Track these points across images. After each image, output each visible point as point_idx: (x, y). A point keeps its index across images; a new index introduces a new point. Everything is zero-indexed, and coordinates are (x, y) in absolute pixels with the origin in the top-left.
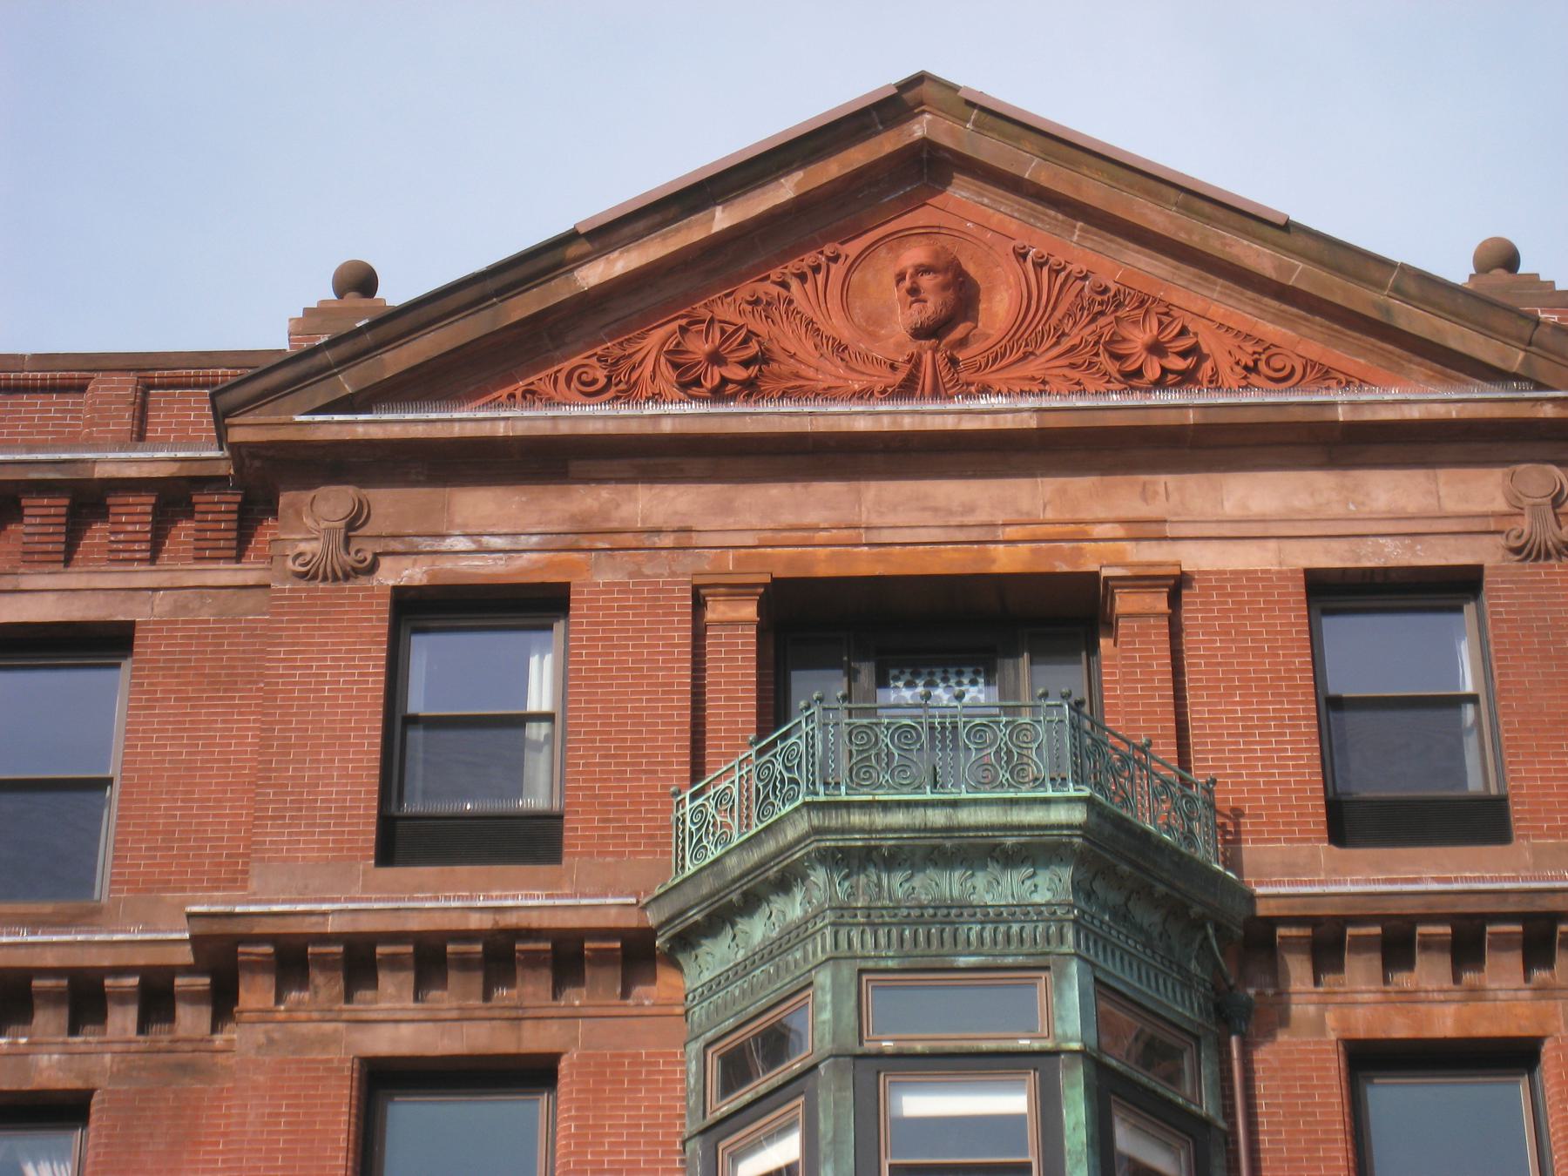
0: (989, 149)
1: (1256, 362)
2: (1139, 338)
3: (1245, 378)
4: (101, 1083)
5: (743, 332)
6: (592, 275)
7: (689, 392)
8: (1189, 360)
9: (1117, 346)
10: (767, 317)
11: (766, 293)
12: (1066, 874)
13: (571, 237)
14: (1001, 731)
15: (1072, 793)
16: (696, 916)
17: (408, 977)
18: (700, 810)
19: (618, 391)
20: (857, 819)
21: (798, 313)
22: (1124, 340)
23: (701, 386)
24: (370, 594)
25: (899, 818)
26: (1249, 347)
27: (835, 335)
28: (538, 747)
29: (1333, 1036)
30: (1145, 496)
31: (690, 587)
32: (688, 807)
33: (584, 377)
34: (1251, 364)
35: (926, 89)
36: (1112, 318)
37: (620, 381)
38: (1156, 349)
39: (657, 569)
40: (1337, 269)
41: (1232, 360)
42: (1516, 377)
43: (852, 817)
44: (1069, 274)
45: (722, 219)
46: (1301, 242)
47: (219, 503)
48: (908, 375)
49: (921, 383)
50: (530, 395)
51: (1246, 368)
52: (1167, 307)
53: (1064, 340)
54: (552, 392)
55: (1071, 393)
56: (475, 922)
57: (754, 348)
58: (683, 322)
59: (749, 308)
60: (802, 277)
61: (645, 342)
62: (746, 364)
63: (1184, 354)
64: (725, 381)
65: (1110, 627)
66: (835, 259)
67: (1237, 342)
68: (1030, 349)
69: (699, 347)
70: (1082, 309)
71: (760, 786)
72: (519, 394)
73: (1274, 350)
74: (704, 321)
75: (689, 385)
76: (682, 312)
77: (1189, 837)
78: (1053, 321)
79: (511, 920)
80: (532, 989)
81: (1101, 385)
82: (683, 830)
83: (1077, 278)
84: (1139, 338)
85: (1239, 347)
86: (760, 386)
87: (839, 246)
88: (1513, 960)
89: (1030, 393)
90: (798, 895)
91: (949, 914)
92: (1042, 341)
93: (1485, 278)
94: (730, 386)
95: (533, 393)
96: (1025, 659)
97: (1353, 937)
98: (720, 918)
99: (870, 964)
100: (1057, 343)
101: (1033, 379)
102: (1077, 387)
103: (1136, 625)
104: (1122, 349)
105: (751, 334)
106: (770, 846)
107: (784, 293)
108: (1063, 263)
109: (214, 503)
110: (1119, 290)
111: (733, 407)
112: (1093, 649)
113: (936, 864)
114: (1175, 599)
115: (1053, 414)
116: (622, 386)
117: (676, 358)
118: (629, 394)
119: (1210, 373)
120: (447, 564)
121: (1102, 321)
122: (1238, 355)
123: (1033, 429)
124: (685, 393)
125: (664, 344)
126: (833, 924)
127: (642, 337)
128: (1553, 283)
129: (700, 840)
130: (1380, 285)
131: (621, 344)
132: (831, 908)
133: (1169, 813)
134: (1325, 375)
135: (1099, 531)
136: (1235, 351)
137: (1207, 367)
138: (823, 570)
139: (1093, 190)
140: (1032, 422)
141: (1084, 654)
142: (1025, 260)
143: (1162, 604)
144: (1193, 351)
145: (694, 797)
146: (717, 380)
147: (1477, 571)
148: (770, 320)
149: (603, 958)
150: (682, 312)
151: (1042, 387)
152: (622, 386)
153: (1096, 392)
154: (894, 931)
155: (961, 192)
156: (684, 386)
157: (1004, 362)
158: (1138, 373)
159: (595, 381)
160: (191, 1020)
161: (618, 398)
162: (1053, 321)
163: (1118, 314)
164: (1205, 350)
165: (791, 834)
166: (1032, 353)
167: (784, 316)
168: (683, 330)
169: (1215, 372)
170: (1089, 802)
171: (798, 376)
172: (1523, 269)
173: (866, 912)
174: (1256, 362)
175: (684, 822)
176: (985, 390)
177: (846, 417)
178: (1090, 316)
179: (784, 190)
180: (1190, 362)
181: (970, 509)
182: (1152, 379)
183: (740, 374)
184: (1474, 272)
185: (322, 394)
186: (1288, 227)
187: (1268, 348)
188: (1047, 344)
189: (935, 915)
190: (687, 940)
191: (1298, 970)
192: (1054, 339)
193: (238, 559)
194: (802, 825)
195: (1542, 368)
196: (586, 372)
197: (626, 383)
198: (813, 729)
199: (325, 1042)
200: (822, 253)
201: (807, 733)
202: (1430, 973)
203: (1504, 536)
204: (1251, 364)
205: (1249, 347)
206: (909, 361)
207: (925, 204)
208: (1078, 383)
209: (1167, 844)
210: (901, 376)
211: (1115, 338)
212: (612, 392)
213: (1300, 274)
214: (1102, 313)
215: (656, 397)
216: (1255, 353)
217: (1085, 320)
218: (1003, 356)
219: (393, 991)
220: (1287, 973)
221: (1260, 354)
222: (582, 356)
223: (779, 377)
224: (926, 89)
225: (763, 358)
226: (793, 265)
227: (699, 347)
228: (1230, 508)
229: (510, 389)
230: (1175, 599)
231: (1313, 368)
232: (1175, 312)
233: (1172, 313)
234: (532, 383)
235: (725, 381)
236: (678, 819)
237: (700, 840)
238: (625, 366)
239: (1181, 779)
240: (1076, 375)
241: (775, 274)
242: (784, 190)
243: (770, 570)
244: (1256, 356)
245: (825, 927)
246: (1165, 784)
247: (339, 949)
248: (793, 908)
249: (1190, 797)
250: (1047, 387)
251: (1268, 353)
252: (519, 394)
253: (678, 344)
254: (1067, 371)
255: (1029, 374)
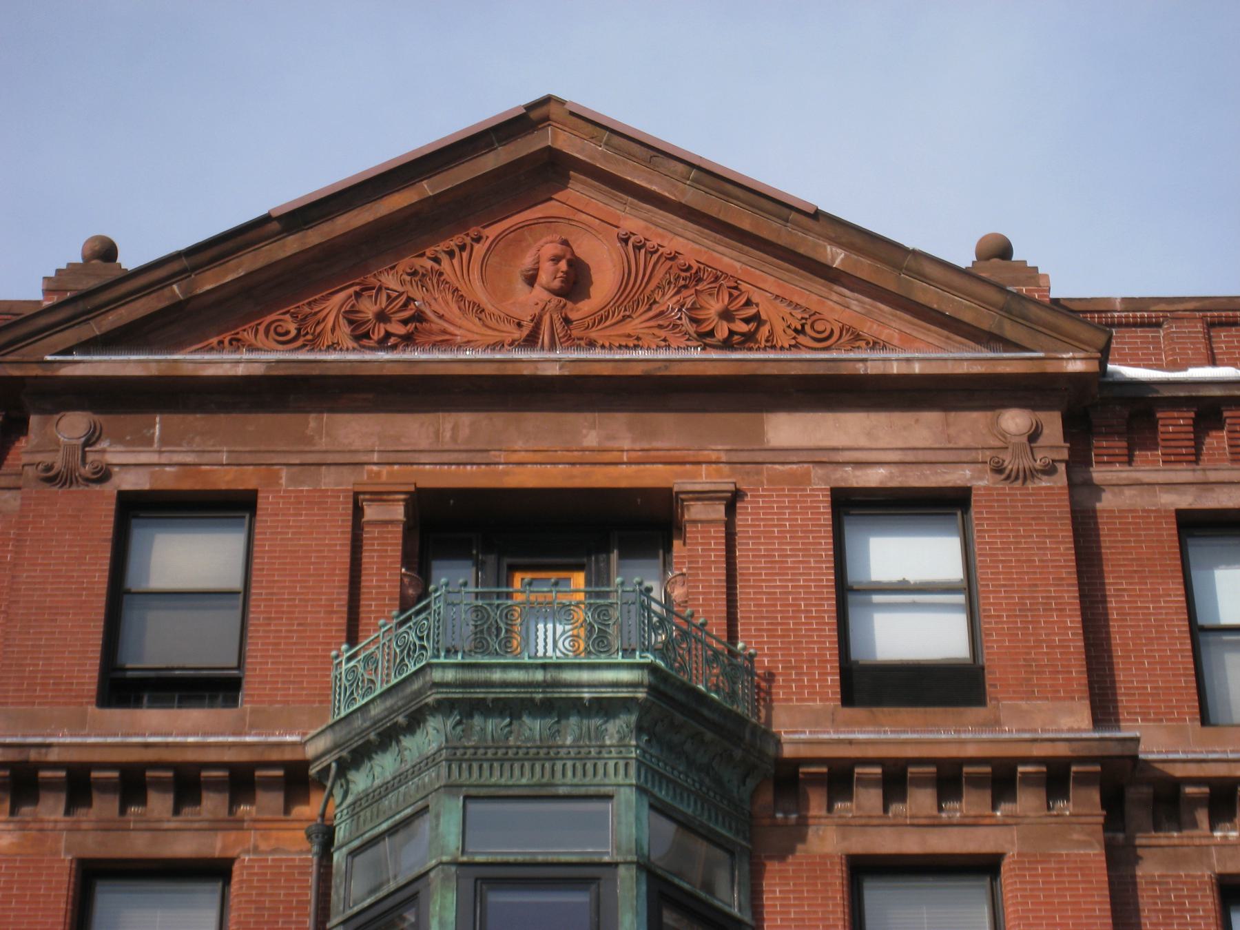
1: (803, 326)
2: (714, 306)
3: (794, 338)
5: (404, 298)
7: (361, 342)
8: (408, 327)
9: (698, 312)
10: (422, 286)
11: (422, 266)
14: (493, 611)
15: (638, 660)
17: (63, 798)
18: (353, 670)
19: (305, 341)
21: (447, 283)
22: (702, 308)
23: (371, 339)
26: (798, 314)
27: (476, 301)
31: (352, 494)
32: (344, 667)
33: (279, 330)
34: (799, 327)
36: (693, 291)
37: (307, 333)
38: (726, 315)
41: (785, 325)
43: (433, 674)
44: (662, 254)
47: (1179, 418)
48: (531, 332)
49: (541, 337)
50: (236, 344)
51: (796, 330)
52: (736, 282)
53: (655, 306)
54: (253, 341)
55: (659, 347)
57: (751, 311)
58: (357, 288)
59: (408, 278)
60: (451, 254)
61: (328, 303)
62: (405, 322)
63: (747, 321)
64: (388, 335)
66: (478, 240)
67: (789, 309)
68: (627, 313)
70: (670, 283)
71: (398, 650)
72: (226, 341)
73: (817, 316)
74: (373, 288)
75: (361, 336)
76: (357, 281)
77: (732, 695)
78: (648, 292)
80: (972, 803)
81: (683, 342)
82: (340, 687)
83: (667, 259)
85: (791, 314)
86: (415, 340)
87: (481, 230)
89: (627, 347)
92: (637, 308)
93: (983, 264)
94: (736, 337)
95: (238, 340)
96: (615, 555)
97: (1022, 773)
99: (473, 792)
100: (650, 309)
101: (629, 336)
102: (663, 343)
103: (376, 532)
104: (701, 315)
105: (410, 300)
107: (436, 266)
108: (656, 246)
109: (1175, 418)
110: (699, 268)
112: (668, 549)
113: (629, 711)
114: (731, 509)
115: (822, 364)
116: (309, 337)
118: (313, 345)
119: (767, 334)
121: (685, 293)
122: (790, 320)
123: (916, 374)
124: (358, 343)
125: (342, 306)
126: (447, 760)
127: (326, 298)
128: (1036, 268)
129: (352, 693)
131: (309, 304)
132: (447, 748)
133: (718, 677)
134: (856, 338)
136: (787, 317)
141: (661, 552)
142: (627, 244)
143: (719, 511)
144: (756, 319)
145: (349, 659)
146: (382, 333)
148: (424, 289)
149: (105, 786)
150: (357, 281)
151: (636, 342)
152: (309, 337)
153: (678, 347)
154: (548, 765)
155: (578, 192)
157: (608, 323)
158: (711, 333)
159: (287, 333)
161: (304, 346)
162: (648, 292)
163: (698, 288)
164: (764, 317)
166: (629, 316)
167: (435, 284)
168: (358, 295)
169: (771, 333)
170: (652, 668)
171: (445, 332)
172: (1016, 257)
173: (597, 749)
174: (803, 326)
175: (340, 679)
176: (591, 344)
177: (953, 362)
178: (676, 289)
180: (752, 326)
182: (721, 338)
183: (401, 330)
184: (975, 259)
187: (814, 314)
188: (641, 310)
189: (527, 753)
192: (647, 306)
196: (280, 326)
197: (313, 334)
198: (439, 608)
200: (467, 235)
201: (435, 611)
203: (35, 467)
204: (799, 327)
205: (798, 314)
206: (532, 320)
207: (551, 199)
208: (665, 340)
209: (713, 700)
210: (526, 332)
211: (695, 306)
212: (300, 342)
214: (685, 287)
215: (332, 347)
216: (802, 318)
217: (671, 292)
218: (607, 318)
220: (807, 800)
221: (806, 319)
222: (278, 313)
223: (431, 333)
224: (553, 109)
226: (442, 247)
227: (369, 308)
229: (220, 338)
230: (731, 509)
231: (848, 330)
232: (744, 286)
233: (739, 287)
234: (238, 333)
235: (388, 335)
236: (336, 677)
237: (352, 693)
238: (311, 321)
239: (730, 651)
240: (663, 333)
241: (429, 252)
243: (413, 480)
244: (804, 321)
245: (441, 761)
246: (716, 654)
247: (63, 774)
249: (735, 666)
250: (640, 343)
251: (813, 318)
252: (226, 341)
253: (353, 306)
254: (656, 331)
255: (627, 332)
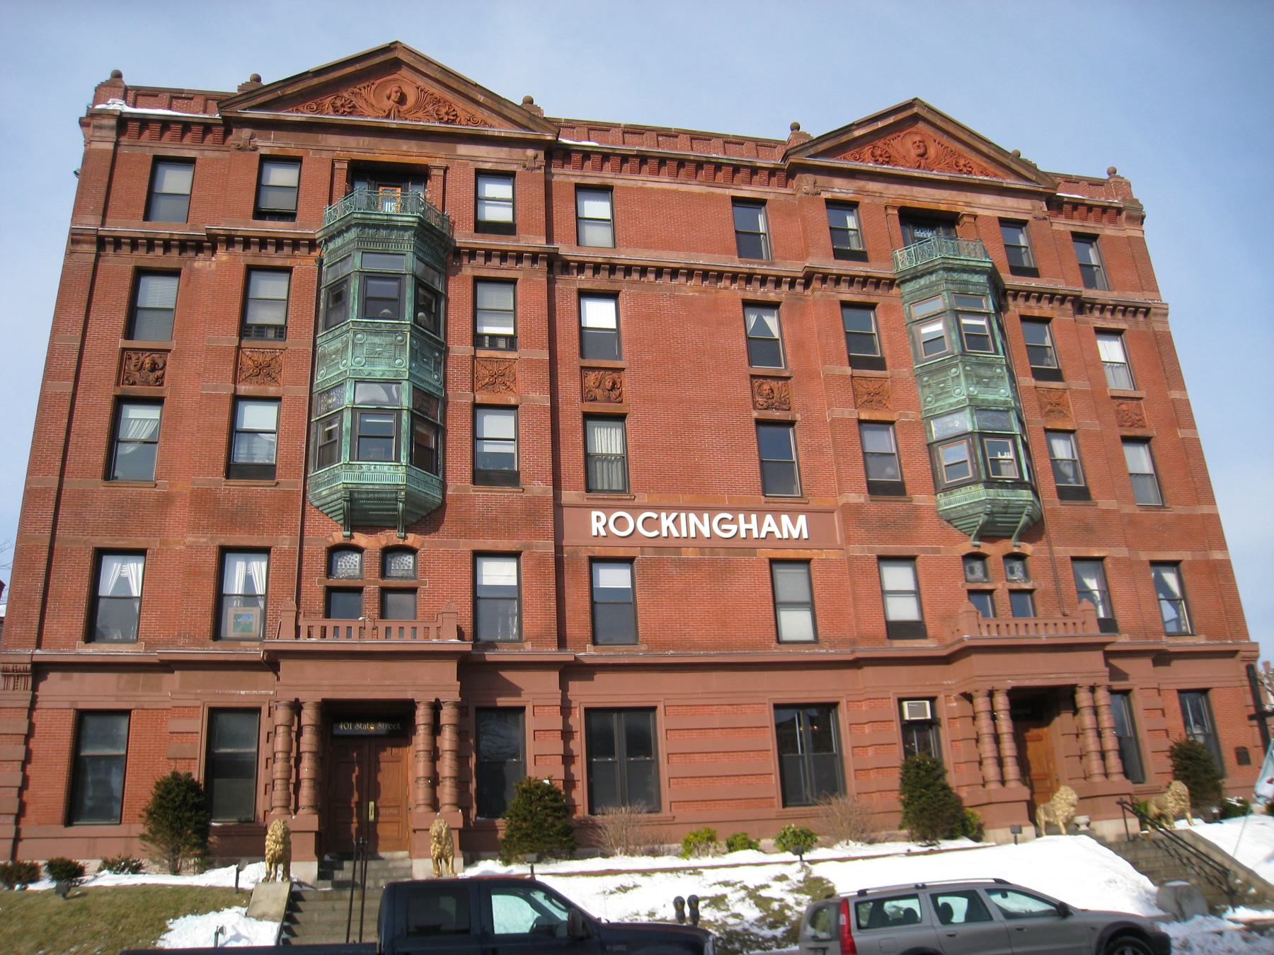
0: (929, 116)
2: (443, 111)
4: (784, 300)
6: (857, 133)
12: (986, 277)
13: (853, 124)
16: (908, 277)
20: (951, 261)
24: (821, 199)
25: (958, 262)
28: (852, 236)
29: (1017, 314)
30: (967, 197)
35: (917, 101)
39: (877, 200)
40: (999, 153)
42: (1034, 181)
45: (880, 124)
46: (993, 146)
50: (297, 111)
56: (862, 274)
60: (365, 88)
62: (350, 108)
63: (453, 116)
64: (344, 111)
65: (430, 178)
66: (373, 84)
69: (339, 103)
75: (336, 111)
79: (869, 274)
80: (510, 263)
84: (962, 162)
88: (1047, 302)
90: (934, 276)
91: (966, 283)
98: (915, 277)
103: (339, 171)
106: (931, 265)
111: (885, 166)
112: (954, 227)
114: (445, 172)
117: (873, 155)
120: (834, 194)
130: (1008, 158)
135: (960, 203)
137: (459, 119)
138: (909, 205)
139: (951, 129)
140: (948, 179)
147: (1027, 221)
156: (335, 112)
158: (442, 119)
160: (799, 288)
165: (936, 263)
168: (335, 98)
176: (406, 119)
179: (891, 120)
181: (934, 195)
185: (812, 151)
186: (990, 143)
190: (903, 282)
191: (1010, 300)
193: (786, 187)
194: (940, 261)
195: (1039, 180)
199: (833, 296)
202: (1032, 302)
213: (992, 153)
219: (495, 262)
224: (917, 101)
225: (889, 157)
227: (339, 103)
228: (982, 202)
230: (445, 172)
235: (344, 111)
242: (891, 120)
246: (438, 215)
248: (934, 278)
